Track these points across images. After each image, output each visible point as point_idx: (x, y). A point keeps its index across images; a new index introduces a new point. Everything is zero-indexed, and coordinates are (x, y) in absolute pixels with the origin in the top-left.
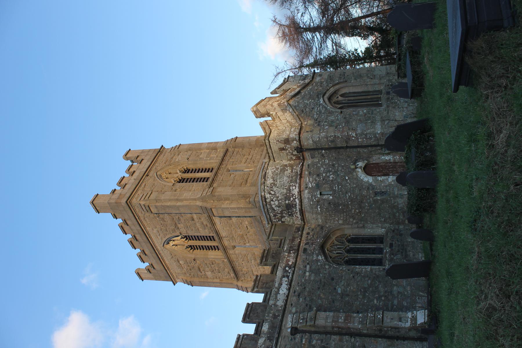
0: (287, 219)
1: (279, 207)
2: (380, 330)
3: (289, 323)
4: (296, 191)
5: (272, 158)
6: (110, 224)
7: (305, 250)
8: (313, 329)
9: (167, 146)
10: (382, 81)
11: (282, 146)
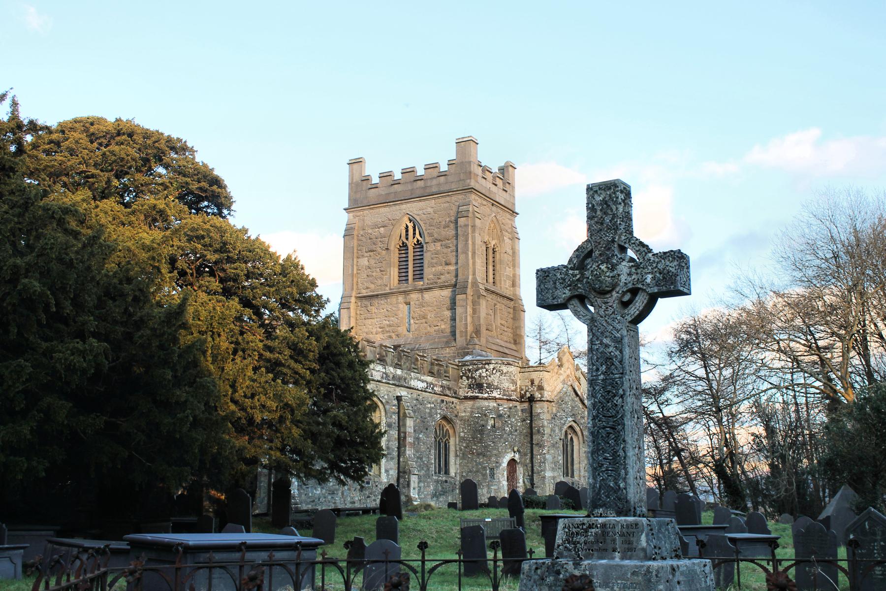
0: (465, 382)
1: (480, 376)
2: (405, 472)
3: (403, 392)
4: (495, 394)
5: (523, 370)
6: (444, 155)
7: (442, 401)
8: (401, 415)
9: (518, 221)
10: (582, 479)
11: (536, 383)
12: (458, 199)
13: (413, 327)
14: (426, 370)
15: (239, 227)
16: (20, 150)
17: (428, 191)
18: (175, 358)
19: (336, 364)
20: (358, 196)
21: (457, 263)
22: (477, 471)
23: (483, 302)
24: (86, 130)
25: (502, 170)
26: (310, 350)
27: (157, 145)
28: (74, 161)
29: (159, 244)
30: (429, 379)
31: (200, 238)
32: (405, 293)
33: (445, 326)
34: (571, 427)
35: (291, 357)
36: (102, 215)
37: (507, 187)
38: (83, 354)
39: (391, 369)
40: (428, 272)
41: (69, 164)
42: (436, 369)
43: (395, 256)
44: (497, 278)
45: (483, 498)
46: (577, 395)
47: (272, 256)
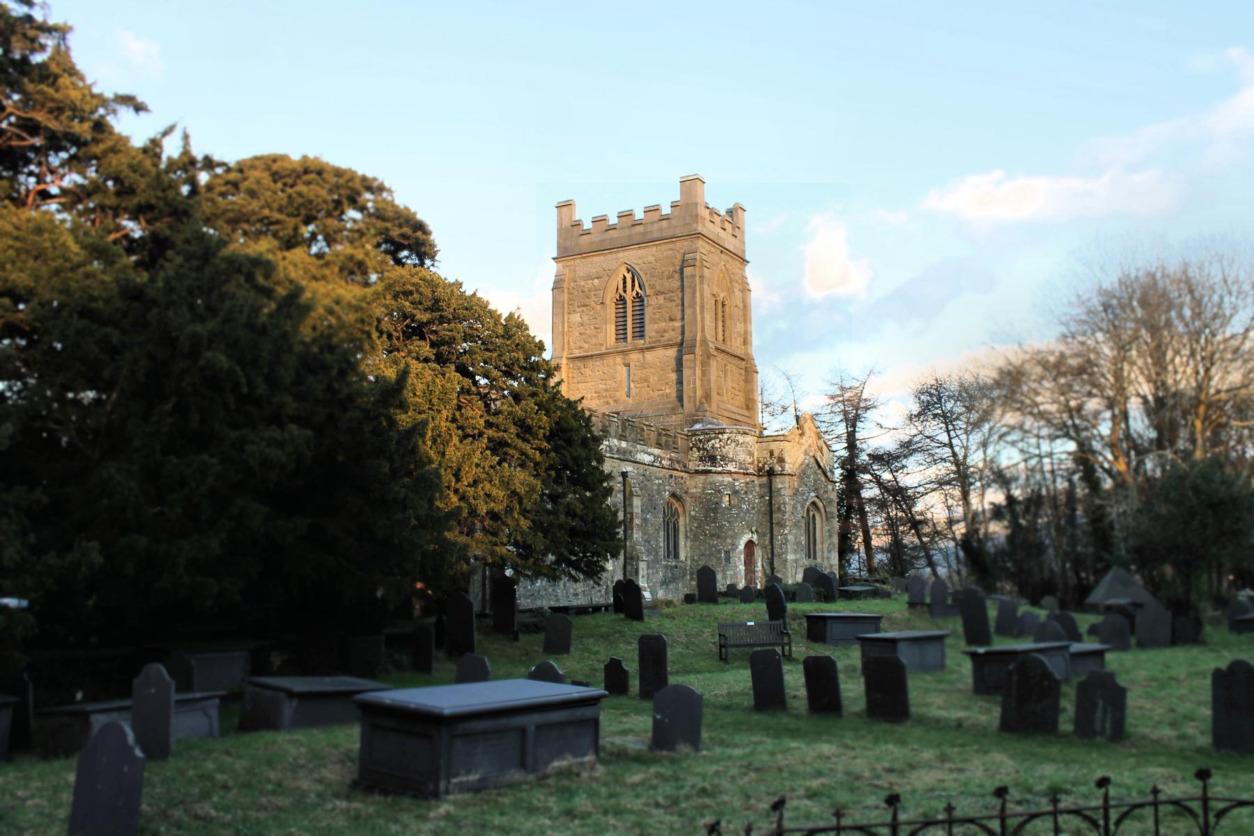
2: (632, 558)
3: (629, 468)
4: (731, 467)
6: (666, 197)
7: (671, 476)
9: (749, 271)
11: (776, 454)
12: (682, 245)
13: (633, 392)
14: (653, 441)
15: (451, 280)
16: (194, 191)
17: (648, 237)
18: (393, 447)
19: (569, 443)
20: (568, 243)
21: (683, 319)
22: (710, 555)
23: (713, 363)
24: (268, 168)
25: (730, 212)
26: (540, 427)
27: (350, 184)
28: (255, 205)
29: (369, 303)
30: (657, 451)
31: (408, 294)
32: (624, 353)
33: (671, 391)
34: (814, 503)
35: (518, 435)
36: (291, 268)
37: (737, 232)
38: (280, 444)
39: (616, 441)
40: (650, 329)
41: (250, 208)
42: (664, 440)
43: (611, 311)
44: (727, 335)
45: (721, 586)
46: (819, 467)
47: (492, 314)
